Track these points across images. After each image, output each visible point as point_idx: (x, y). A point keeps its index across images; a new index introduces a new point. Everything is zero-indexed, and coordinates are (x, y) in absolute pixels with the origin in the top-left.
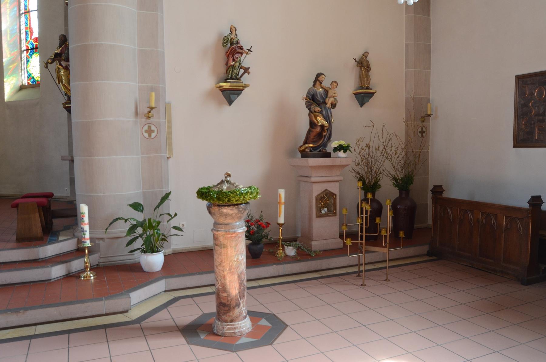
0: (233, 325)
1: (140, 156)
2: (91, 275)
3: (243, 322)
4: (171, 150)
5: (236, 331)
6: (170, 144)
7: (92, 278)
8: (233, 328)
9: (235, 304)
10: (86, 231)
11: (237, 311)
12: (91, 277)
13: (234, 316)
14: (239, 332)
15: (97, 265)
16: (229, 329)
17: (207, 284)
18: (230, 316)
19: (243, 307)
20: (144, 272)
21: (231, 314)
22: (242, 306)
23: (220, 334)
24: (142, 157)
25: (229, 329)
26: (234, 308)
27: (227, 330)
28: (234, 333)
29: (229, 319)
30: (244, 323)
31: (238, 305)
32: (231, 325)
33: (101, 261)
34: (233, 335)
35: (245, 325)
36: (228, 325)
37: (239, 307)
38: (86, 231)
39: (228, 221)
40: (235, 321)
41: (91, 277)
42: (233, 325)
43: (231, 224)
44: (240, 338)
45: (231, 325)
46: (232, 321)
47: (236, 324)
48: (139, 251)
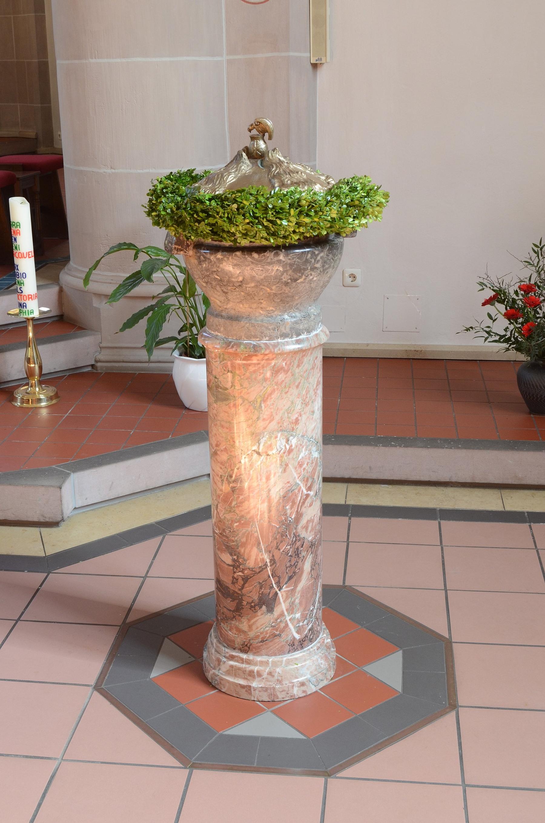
0: (248, 662)
1: (225, 58)
2: (42, 397)
3: (285, 658)
4: (321, 39)
5: (254, 684)
6: (320, 22)
7: (43, 404)
8: (244, 671)
9: (256, 598)
10: (24, 275)
11: (263, 621)
12: (39, 400)
13: (251, 634)
14: (265, 689)
15: (93, 366)
16: (233, 671)
17: (338, 475)
18: (239, 631)
19: (291, 610)
20: (180, 405)
21: (244, 625)
22: (282, 606)
23: (209, 675)
24: (229, 62)
25: (233, 671)
26: (254, 607)
27: (228, 673)
28: (248, 688)
29: (239, 640)
30: (288, 662)
31: (268, 602)
32: (242, 661)
33: (101, 357)
34: (244, 694)
35: (301, 667)
36: (232, 658)
37: (270, 610)
38: (24, 275)
39: (243, 308)
40: (257, 651)
41: (39, 400)
42: (248, 662)
43: (249, 318)
44: (258, 711)
45: (242, 661)
46: (246, 648)
47: (259, 662)
48: (172, 344)
